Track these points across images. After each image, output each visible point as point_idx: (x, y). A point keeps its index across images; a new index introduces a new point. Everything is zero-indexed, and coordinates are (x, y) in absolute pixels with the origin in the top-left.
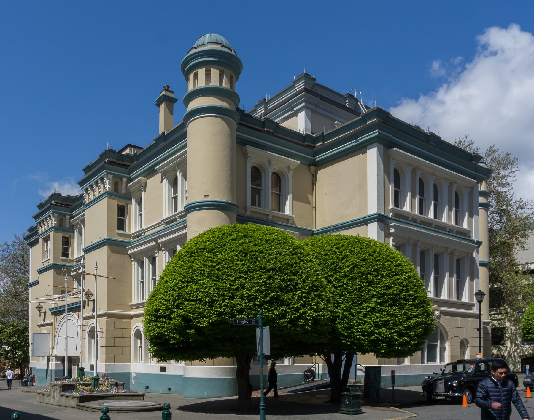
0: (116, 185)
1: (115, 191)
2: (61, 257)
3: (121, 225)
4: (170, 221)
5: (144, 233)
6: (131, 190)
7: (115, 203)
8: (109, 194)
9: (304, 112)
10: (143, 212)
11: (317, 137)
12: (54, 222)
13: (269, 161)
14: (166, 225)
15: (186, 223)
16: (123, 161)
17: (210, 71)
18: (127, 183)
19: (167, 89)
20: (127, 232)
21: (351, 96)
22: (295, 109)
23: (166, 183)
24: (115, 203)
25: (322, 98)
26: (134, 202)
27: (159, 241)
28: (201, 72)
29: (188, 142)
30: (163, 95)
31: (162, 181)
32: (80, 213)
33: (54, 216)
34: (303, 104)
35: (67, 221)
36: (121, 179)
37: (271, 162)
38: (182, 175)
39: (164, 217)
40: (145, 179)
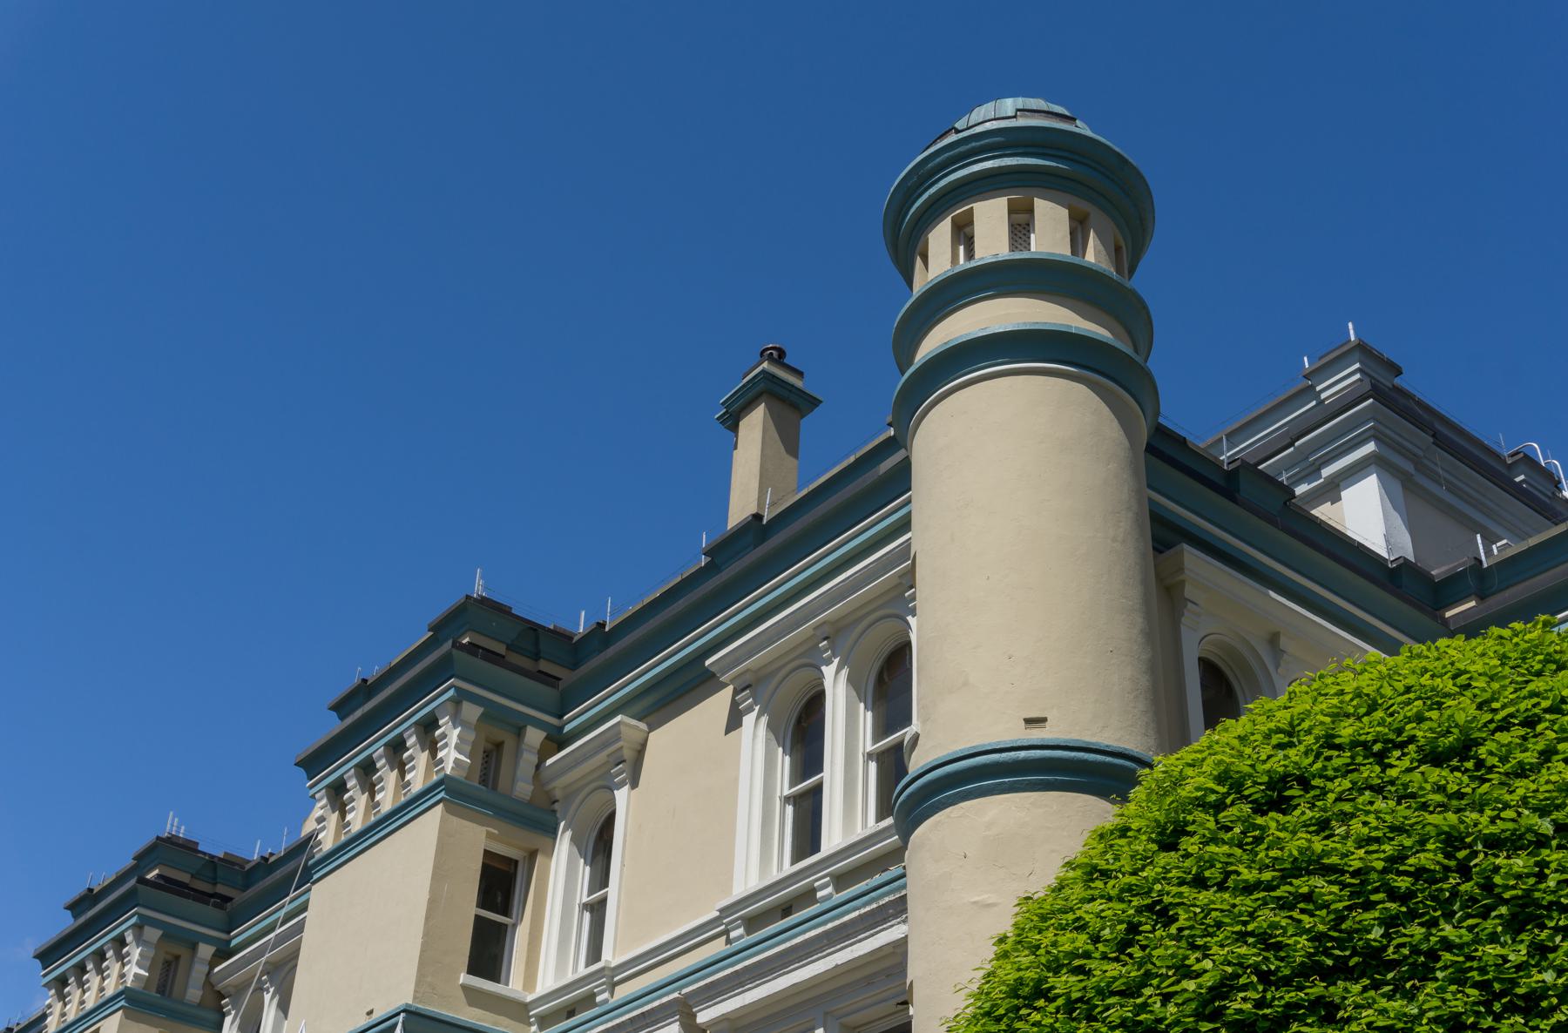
0: (490, 756)
1: (484, 781)
2: (464, 978)
3: (488, 952)
4: (770, 911)
5: (612, 987)
6: (558, 786)
7: (476, 838)
8: (453, 793)
9: (1374, 476)
10: (612, 891)
11: (1453, 579)
12: (133, 970)
13: (1273, 640)
14: (749, 932)
15: (904, 886)
16: (536, 657)
17: (1031, 211)
18: (544, 754)
19: (779, 357)
20: (514, 985)
21: (1529, 461)
22: (1327, 472)
23: (754, 729)
24: (476, 838)
25: (1440, 441)
26: (564, 845)
27: (703, 1017)
28: (991, 216)
29: (915, 507)
30: (763, 371)
31: (734, 722)
32: (271, 929)
33: (139, 940)
34: (1371, 447)
35: (200, 970)
36: (519, 733)
37: (1284, 642)
38: (850, 680)
39: (739, 890)
40: (643, 726)
